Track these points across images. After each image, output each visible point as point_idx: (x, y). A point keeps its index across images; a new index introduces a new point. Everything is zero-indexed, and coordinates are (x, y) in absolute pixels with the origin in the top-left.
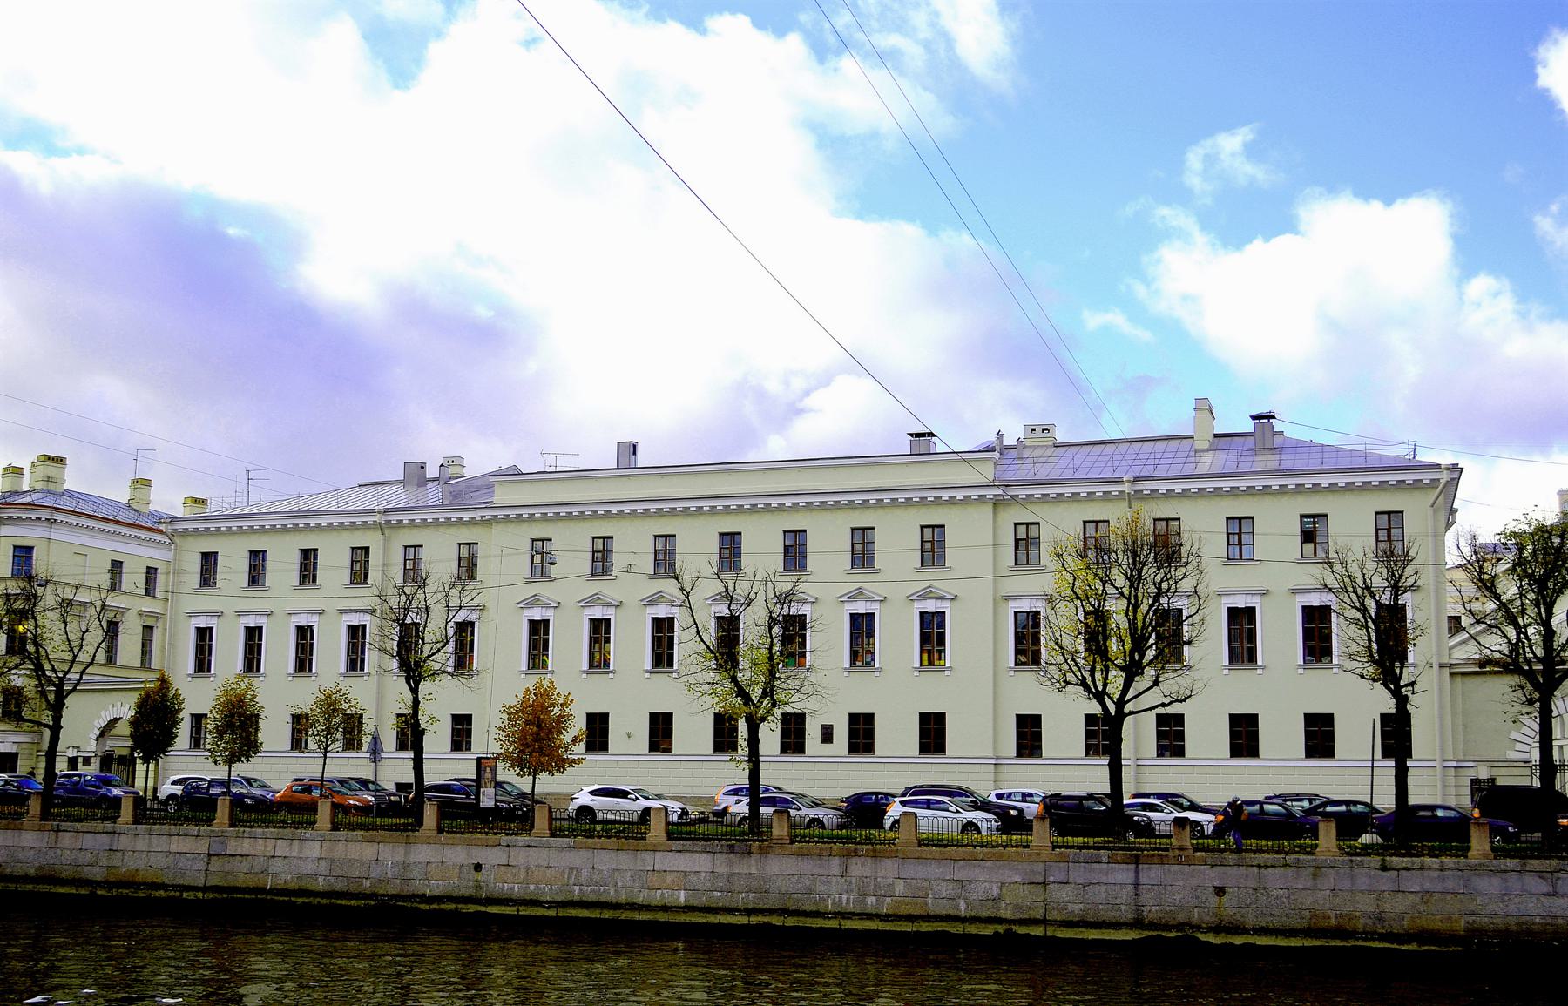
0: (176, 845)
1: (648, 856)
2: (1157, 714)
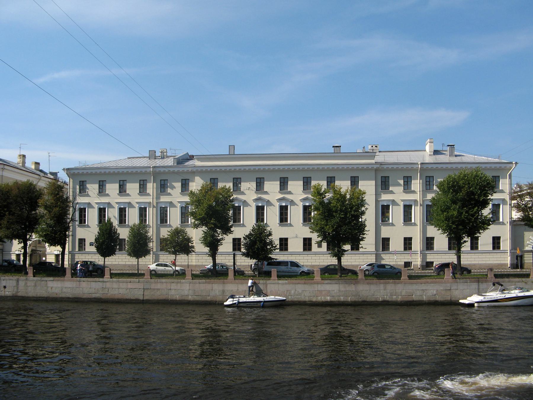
0: (130, 286)
1: (316, 286)
2: (241, 238)
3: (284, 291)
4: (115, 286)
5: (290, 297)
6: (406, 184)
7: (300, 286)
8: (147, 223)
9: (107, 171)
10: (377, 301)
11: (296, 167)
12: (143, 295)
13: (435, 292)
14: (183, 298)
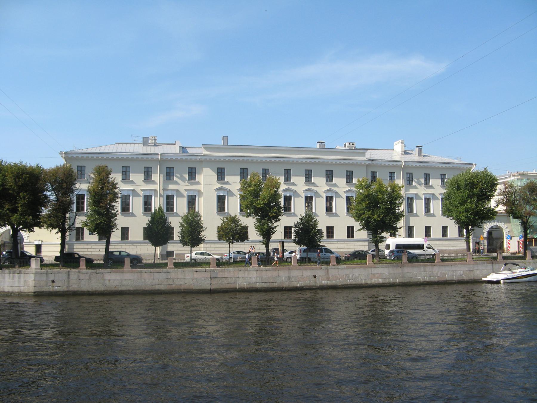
0: (196, 275)
1: (370, 269)
3: (344, 276)
4: (181, 276)
5: (349, 281)
6: (190, 175)
7: (356, 270)
8: (314, 211)
9: (110, 156)
10: (419, 282)
11: (264, 159)
12: (211, 284)
13: (462, 273)
14: (251, 286)
